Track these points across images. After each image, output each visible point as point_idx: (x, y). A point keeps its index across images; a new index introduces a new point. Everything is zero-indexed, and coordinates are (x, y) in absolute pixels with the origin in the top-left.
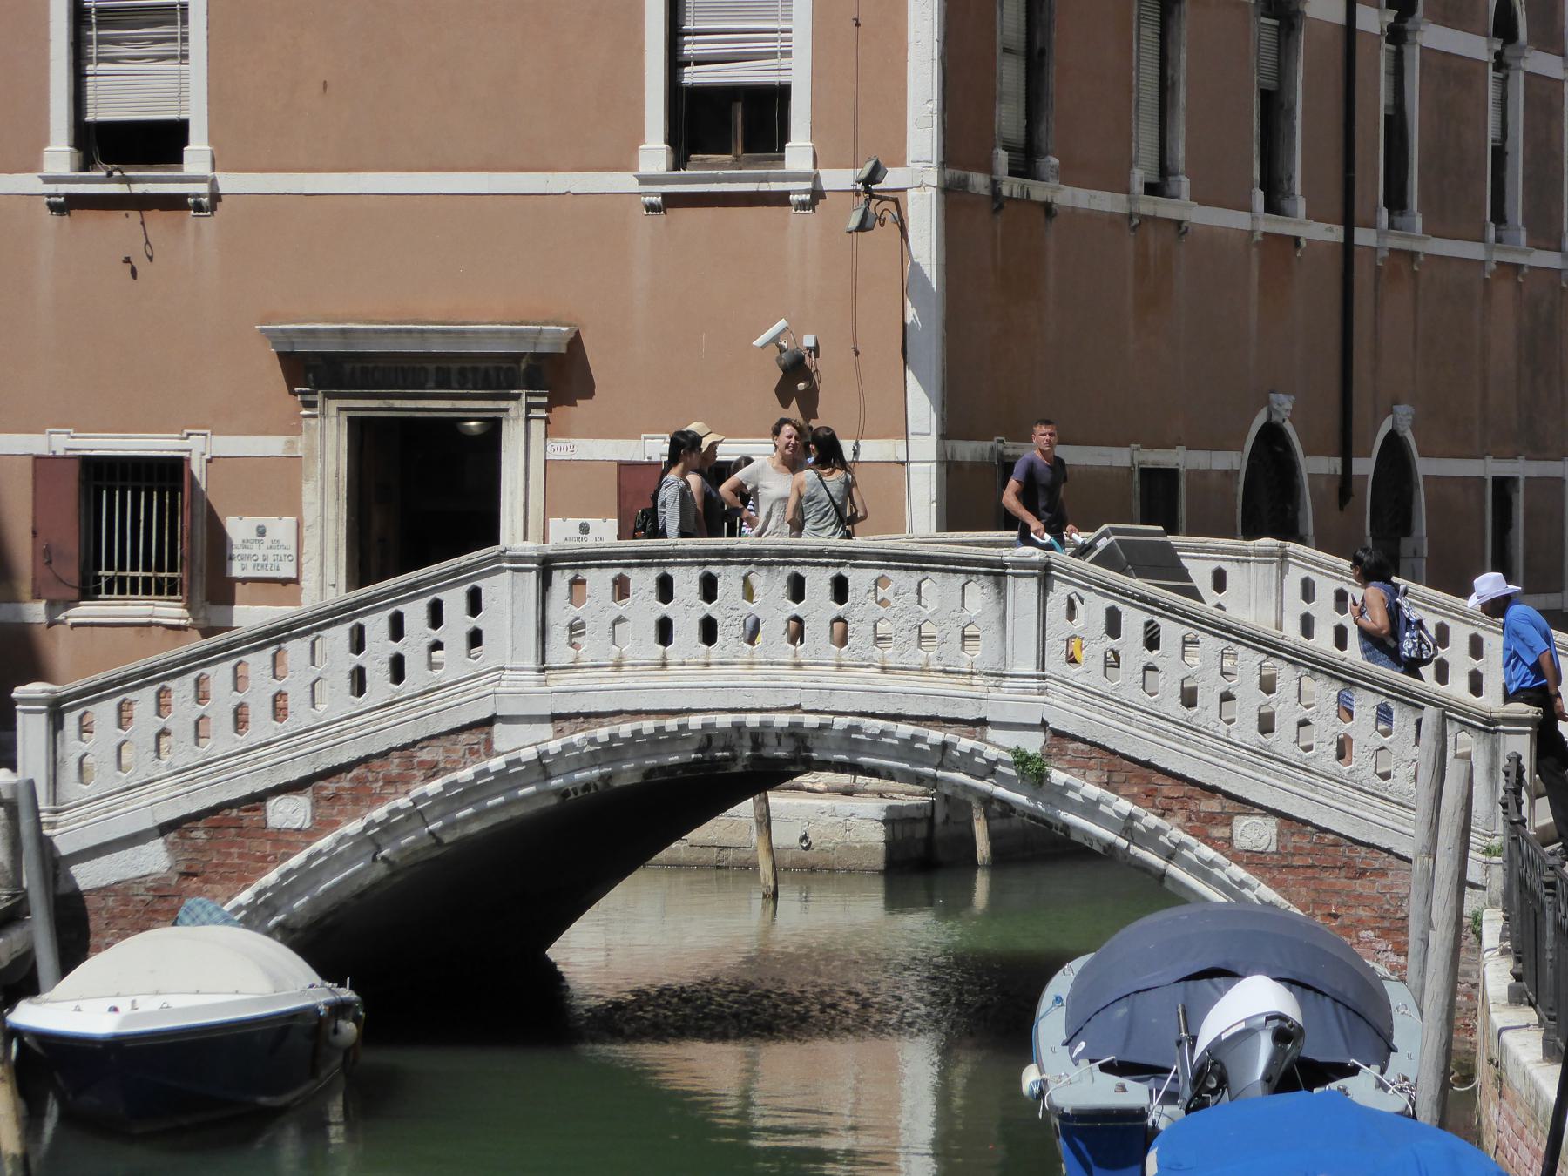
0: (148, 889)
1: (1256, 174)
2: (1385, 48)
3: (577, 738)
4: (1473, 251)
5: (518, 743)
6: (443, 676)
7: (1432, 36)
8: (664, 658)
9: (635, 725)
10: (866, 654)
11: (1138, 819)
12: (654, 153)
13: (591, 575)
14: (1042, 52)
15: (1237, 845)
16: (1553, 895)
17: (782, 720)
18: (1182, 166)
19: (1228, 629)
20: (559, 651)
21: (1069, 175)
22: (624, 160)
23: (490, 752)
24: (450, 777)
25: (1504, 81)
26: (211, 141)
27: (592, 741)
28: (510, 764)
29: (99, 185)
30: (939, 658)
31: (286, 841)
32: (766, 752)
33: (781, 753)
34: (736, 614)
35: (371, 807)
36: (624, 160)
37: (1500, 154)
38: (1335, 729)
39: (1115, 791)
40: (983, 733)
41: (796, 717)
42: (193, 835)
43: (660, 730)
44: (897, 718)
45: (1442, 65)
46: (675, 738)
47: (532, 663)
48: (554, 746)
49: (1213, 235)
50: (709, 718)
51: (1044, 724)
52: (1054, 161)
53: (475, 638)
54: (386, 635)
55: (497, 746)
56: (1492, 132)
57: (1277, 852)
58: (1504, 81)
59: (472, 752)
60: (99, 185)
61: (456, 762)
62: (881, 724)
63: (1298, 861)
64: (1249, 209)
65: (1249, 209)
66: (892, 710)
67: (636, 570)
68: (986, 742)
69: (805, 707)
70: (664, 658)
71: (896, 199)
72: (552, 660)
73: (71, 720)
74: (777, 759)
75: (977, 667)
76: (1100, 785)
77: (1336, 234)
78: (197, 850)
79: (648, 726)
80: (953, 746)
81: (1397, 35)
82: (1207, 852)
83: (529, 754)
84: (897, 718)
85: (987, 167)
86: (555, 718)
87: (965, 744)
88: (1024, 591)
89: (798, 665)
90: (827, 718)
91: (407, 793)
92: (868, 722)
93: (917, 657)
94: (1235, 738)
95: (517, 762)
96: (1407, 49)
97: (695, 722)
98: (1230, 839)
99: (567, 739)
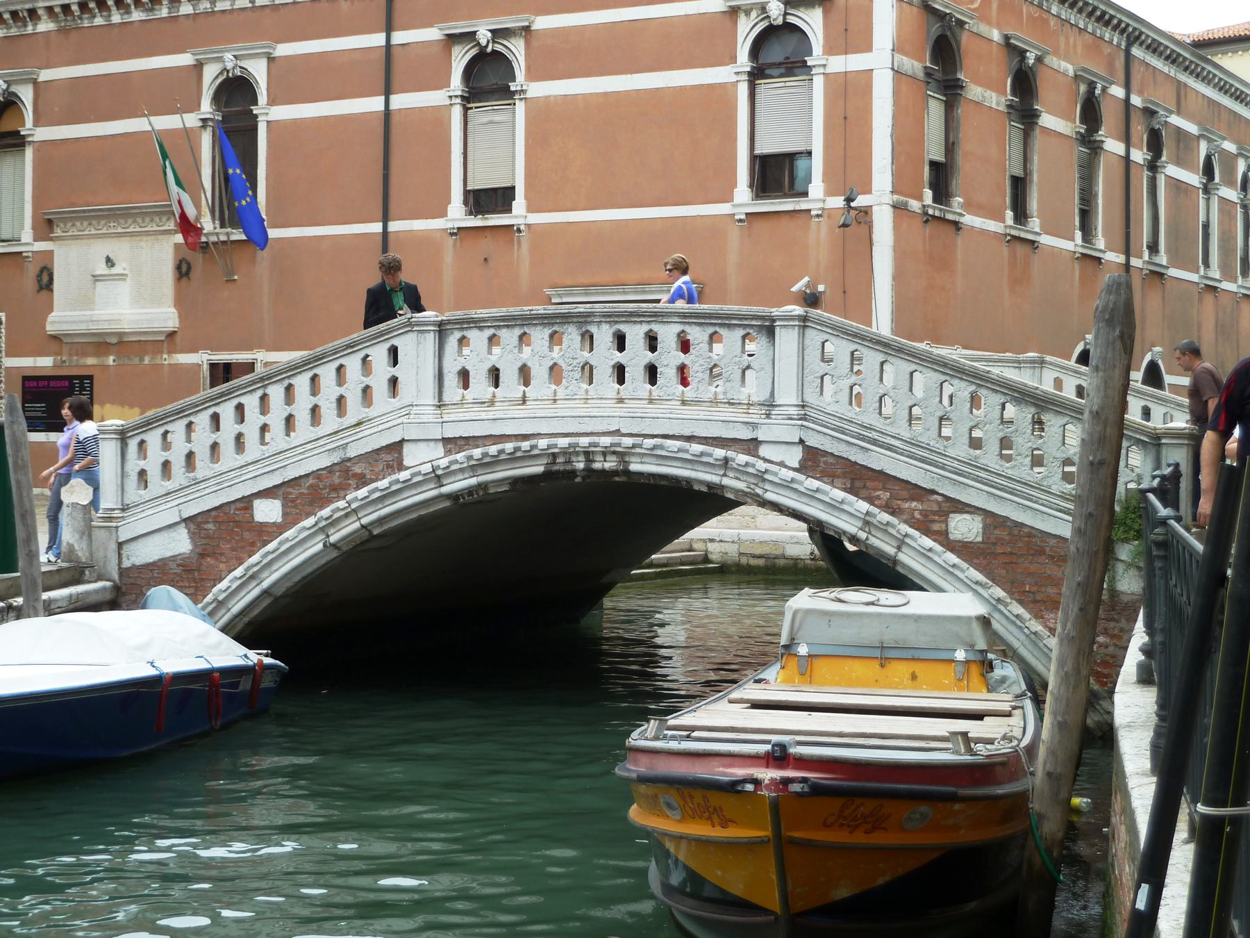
0: (178, 565)
1: (1077, 223)
2: (1146, 173)
3: (460, 456)
4: (1194, 277)
5: (419, 458)
6: (372, 412)
7: (1173, 171)
8: (524, 396)
9: (500, 447)
10: (670, 391)
11: (874, 516)
12: (743, 192)
13: (473, 334)
14: (953, 143)
15: (951, 537)
16: (1165, 558)
17: (606, 441)
18: (1035, 214)
19: (945, 365)
20: (453, 391)
21: (970, 207)
22: (727, 197)
23: (401, 467)
24: (373, 485)
25: (1208, 200)
26: (526, 198)
27: (470, 458)
28: (413, 475)
29: (477, 222)
30: (725, 393)
31: (266, 532)
32: (597, 466)
33: (607, 465)
34: (575, 362)
35: (322, 508)
36: (727, 197)
37: (1206, 226)
38: (1030, 444)
39: (856, 495)
40: (756, 449)
41: (616, 439)
42: (206, 526)
43: (517, 449)
44: (690, 439)
45: (1177, 186)
46: (529, 457)
47: (431, 399)
48: (444, 463)
49: (1054, 252)
50: (553, 441)
51: (801, 441)
52: (960, 200)
53: (394, 381)
54: (334, 383)
55: (406, 463)
56: (1202, 217)
57: (983, 542)
58: (1208, 200)
59: (389, 466)
60: (477, 222)
61: (378, 474)
62: (678, 444)
63: (999, 550)
64: (1073, 240)
65: (1073, 240)
66: (687, 433)
67: (504, 330)
68: (759, 457)
69: (623, 431)
70: (524, 396)
71: (866, 212)
72: (447, 398)
73: (133, 445)
74: (603, 471)
75: (755, 399)
76: (845, 490)
77: (1121, 259)
78: (208, 537)
79: (509, 447)
80: (733, 460)
81: (1153, 166)
82: (927, 542)
83: (427, 468)
84: (690, 439)
85: (920, 198)
86: (446, 441)
87: (742, 458)
88: (787, 338)
89: (621, 401)
90: (638, 440)
91: (344, 498)
92: (669, 442)
93: (708, 392)
94: (951, 452)
95: (419, 473)
96: (1158, 176)
97: (543, 443)
98: (946, 533)
99: (452, 458)
